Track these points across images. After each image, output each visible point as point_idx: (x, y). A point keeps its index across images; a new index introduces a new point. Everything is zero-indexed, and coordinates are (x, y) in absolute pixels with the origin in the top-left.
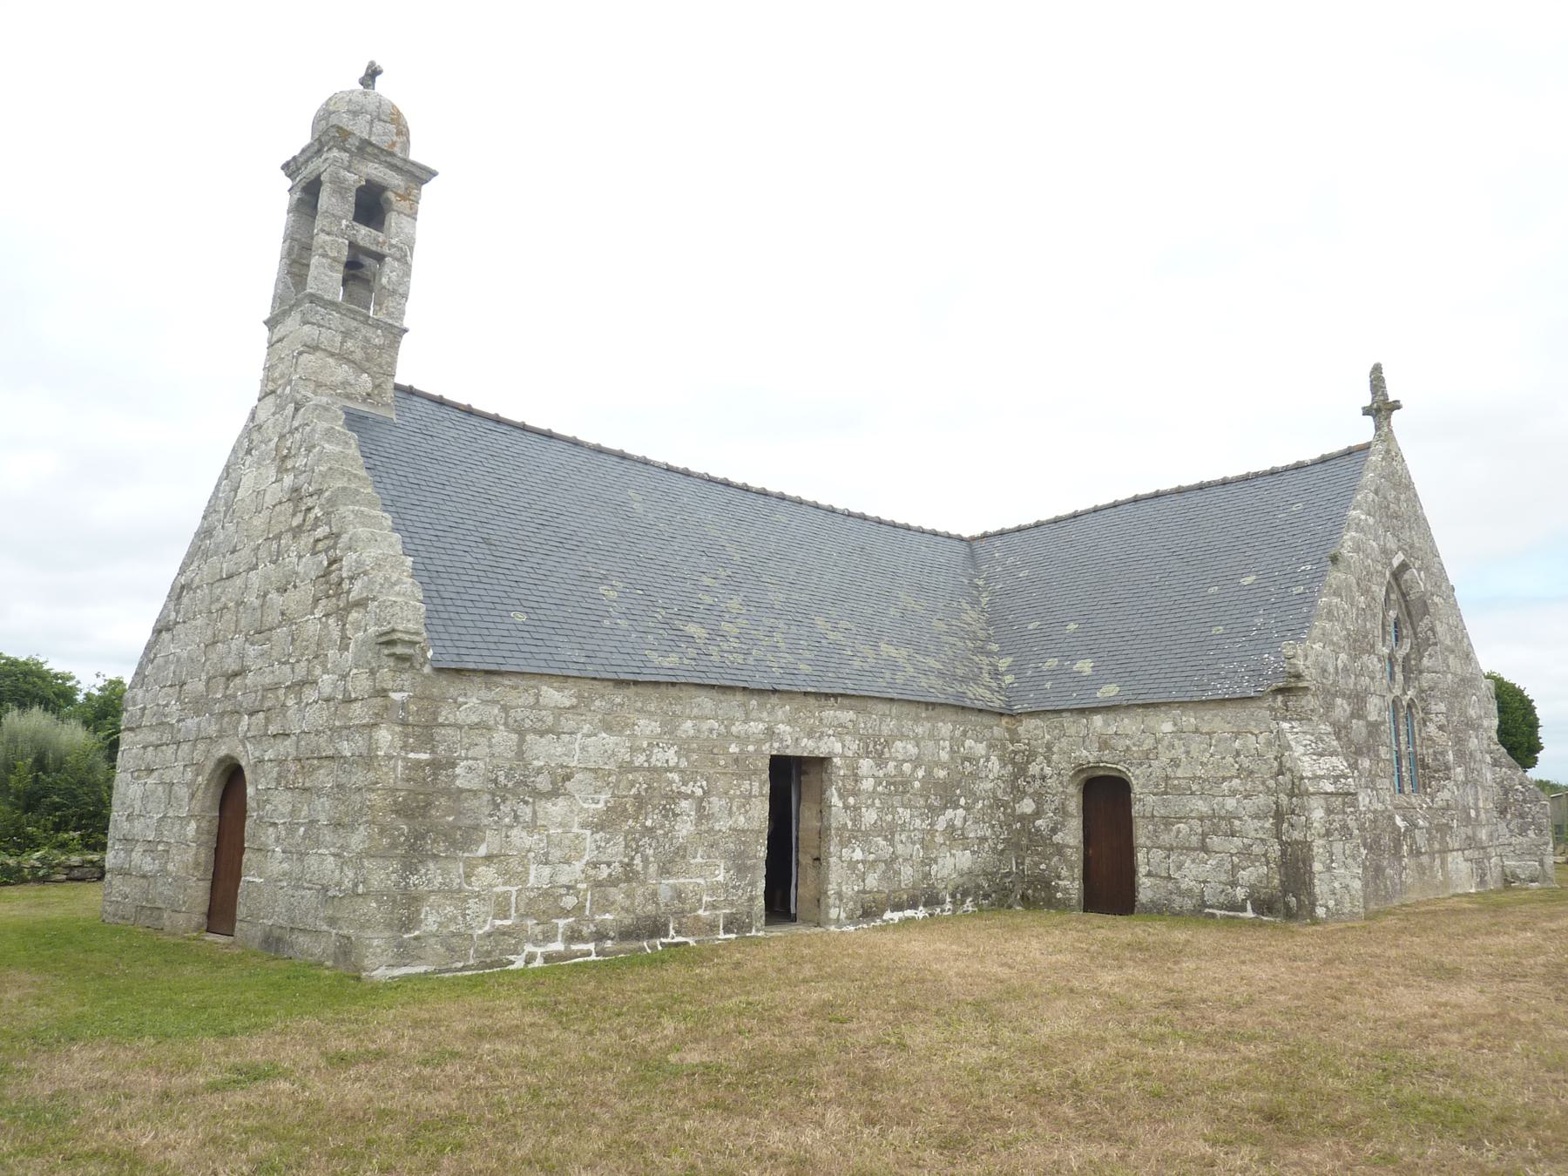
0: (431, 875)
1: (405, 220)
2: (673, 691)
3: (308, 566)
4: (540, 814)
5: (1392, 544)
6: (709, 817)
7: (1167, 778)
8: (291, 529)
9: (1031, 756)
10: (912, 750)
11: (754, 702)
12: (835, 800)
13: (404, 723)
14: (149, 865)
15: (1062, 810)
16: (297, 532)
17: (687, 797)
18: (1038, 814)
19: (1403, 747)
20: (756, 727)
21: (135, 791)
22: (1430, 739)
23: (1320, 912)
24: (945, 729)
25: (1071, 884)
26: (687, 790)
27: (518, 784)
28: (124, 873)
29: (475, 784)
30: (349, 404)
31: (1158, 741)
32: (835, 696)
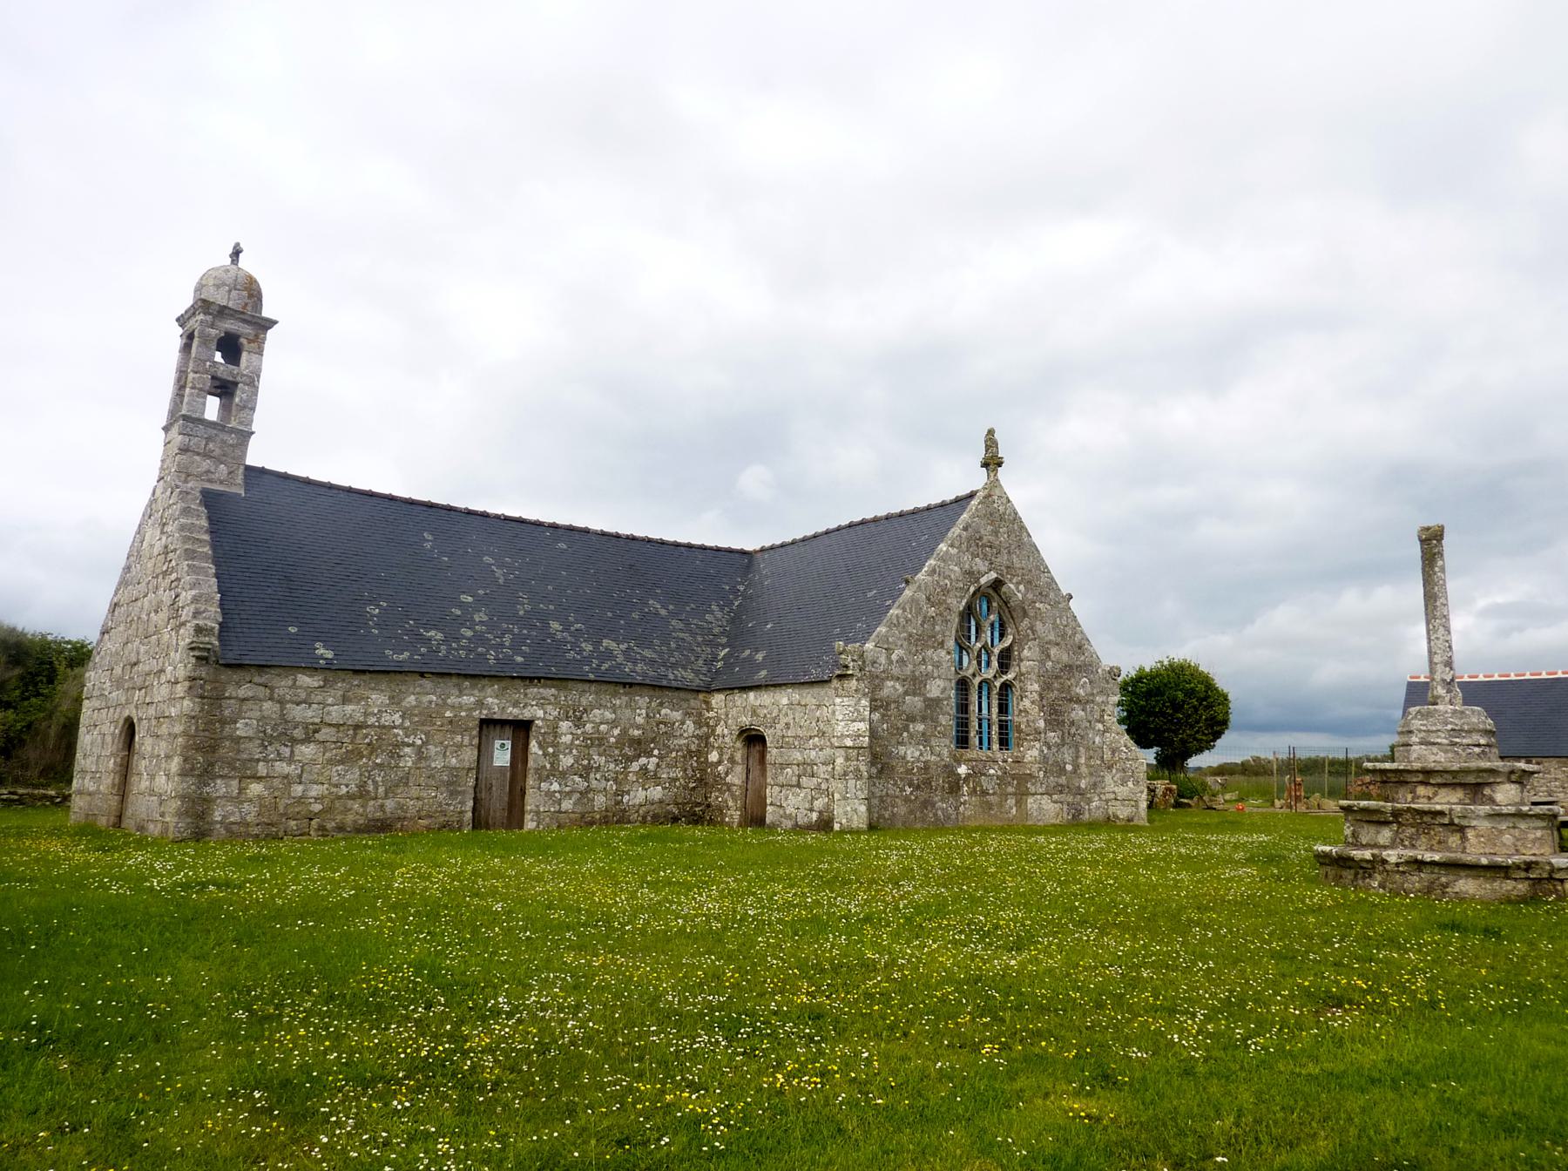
0: (220, 787)
1: (254, 357)
2: (399, 677)
4: (297, 752)
5: (980, 564)
6: (426, 759)
10: (609, 715)
13: (202, 697)
15: (732, 760)
16: (165, 573)
17: (409, 745)
18: (720, 762)
20: (468, 700)
22: (1026, 711)
23: (837, 827)
24: (642, 701)
27: (281, 734)
28: (80, 793)
29: (251, 733)
30: (208, 486)
32: (539, 679)
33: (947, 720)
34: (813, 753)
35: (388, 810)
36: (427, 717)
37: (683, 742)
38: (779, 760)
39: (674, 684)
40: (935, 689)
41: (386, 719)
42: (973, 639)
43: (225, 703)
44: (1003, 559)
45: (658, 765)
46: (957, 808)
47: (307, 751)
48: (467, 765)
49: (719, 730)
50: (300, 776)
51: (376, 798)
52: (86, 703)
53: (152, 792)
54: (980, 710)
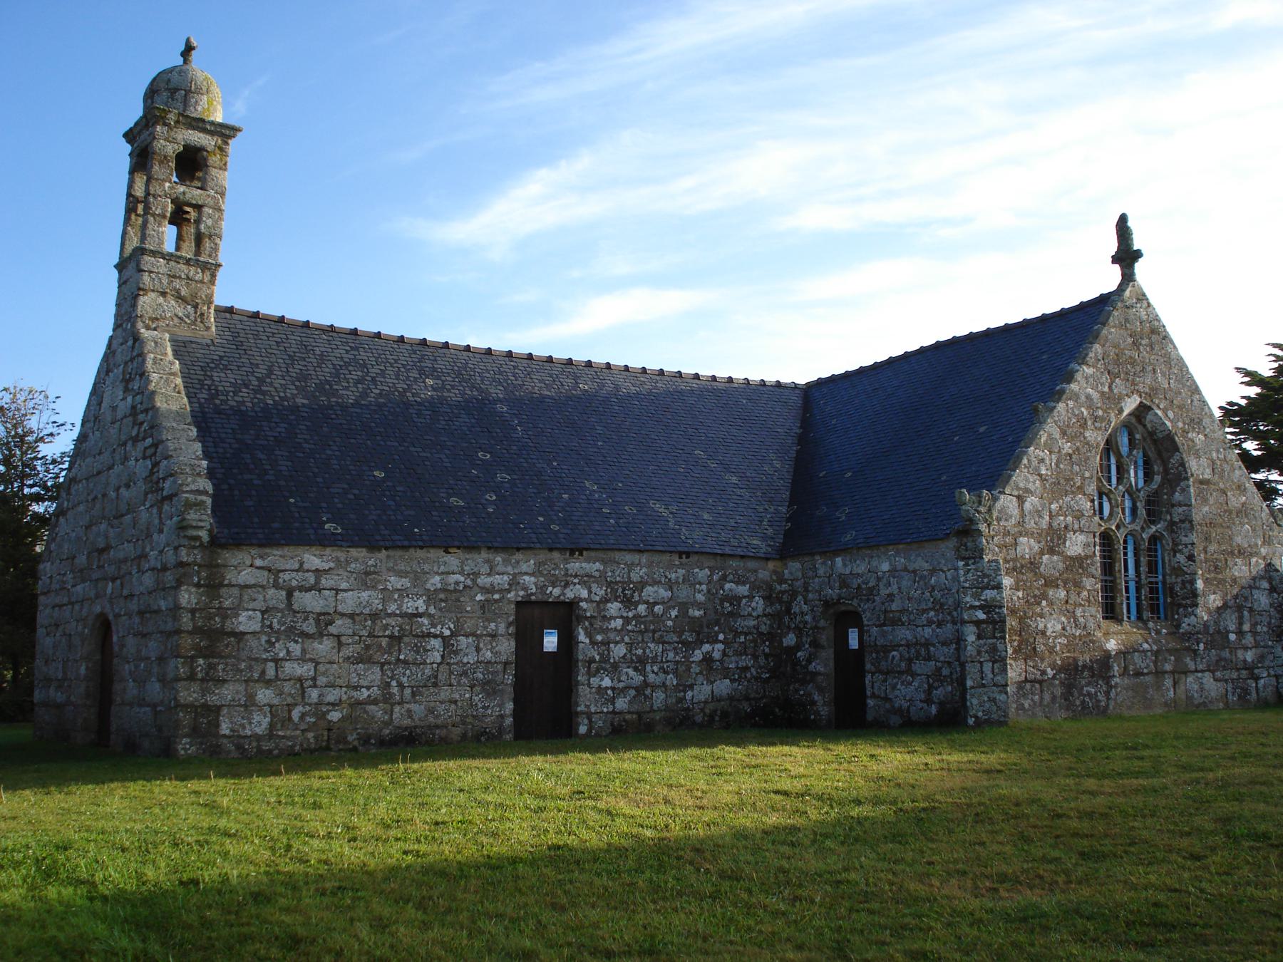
3: (141, 468)
6: (456, 653)
7: (886, 611)
8: (131, 438)
9: (793, 594)
10: (664, 593)
11: (499, 559)
12: (582, 637)
14: (60, 697)
15: (815, 644)
17: (435, 636)
18: (798, 647)
19: (1143, 577)
21: (48, 641)
24: (702, 574)
25: (822, 705)
26: (437, 631)
31: (879, 579)
33: (1092, 584)
34: (928, 631)
35: (416, 717)
36: (448, 598)
37: (752, 623)
38: (881, 642)
39: (739, 551)
40: (1076, 545)
41: (410, 606)
42: (1114, 480)
43: (223, 591)
44: (1146, 382)
45: (724, 654)
46: (1107, 693)
47: (323, 648)
48: (504, 658)
49: (795, 609)
50: (314, 679)
51: (401, 703)
52: (42, 599)
53: (142, 703)
54: (1126, 570)
